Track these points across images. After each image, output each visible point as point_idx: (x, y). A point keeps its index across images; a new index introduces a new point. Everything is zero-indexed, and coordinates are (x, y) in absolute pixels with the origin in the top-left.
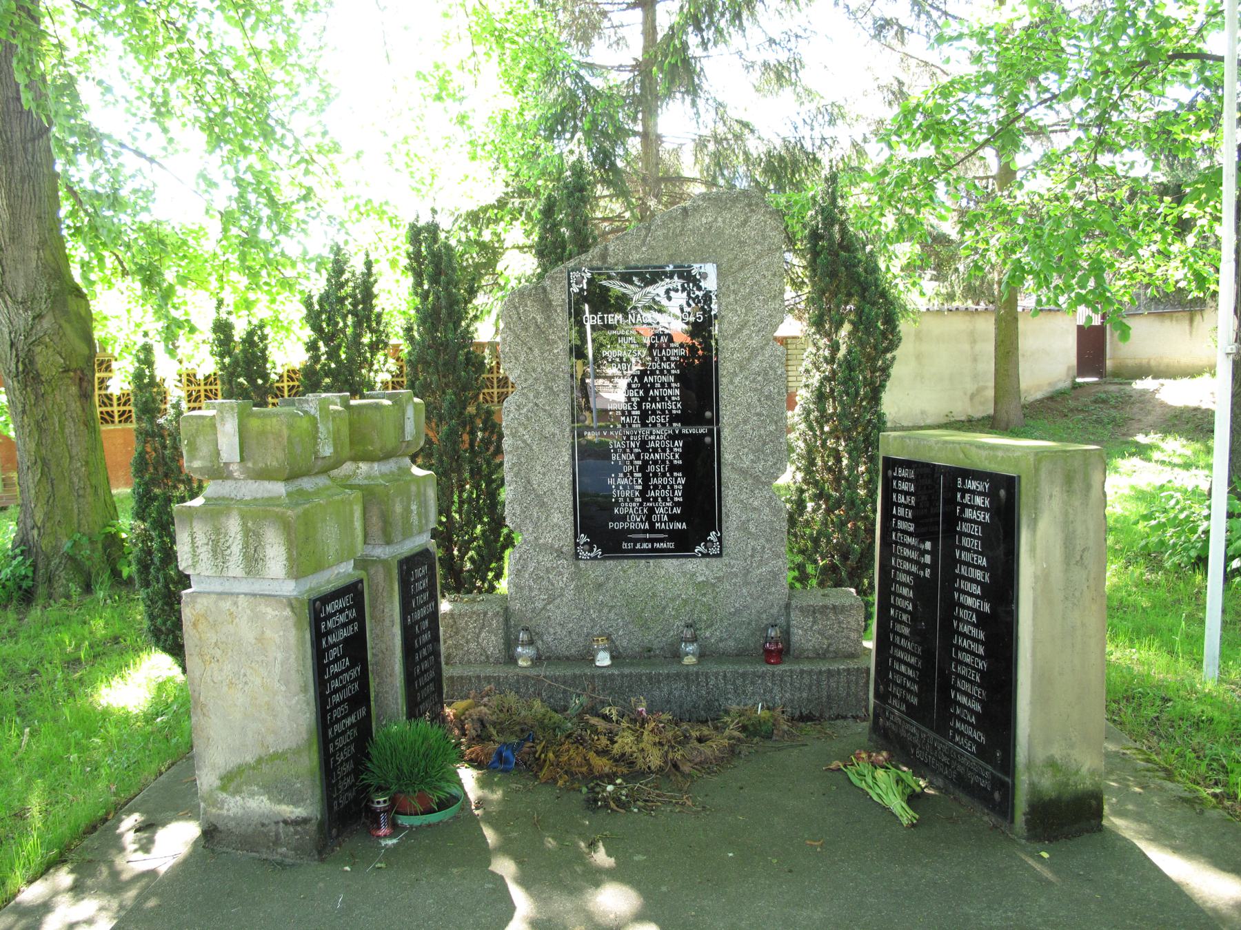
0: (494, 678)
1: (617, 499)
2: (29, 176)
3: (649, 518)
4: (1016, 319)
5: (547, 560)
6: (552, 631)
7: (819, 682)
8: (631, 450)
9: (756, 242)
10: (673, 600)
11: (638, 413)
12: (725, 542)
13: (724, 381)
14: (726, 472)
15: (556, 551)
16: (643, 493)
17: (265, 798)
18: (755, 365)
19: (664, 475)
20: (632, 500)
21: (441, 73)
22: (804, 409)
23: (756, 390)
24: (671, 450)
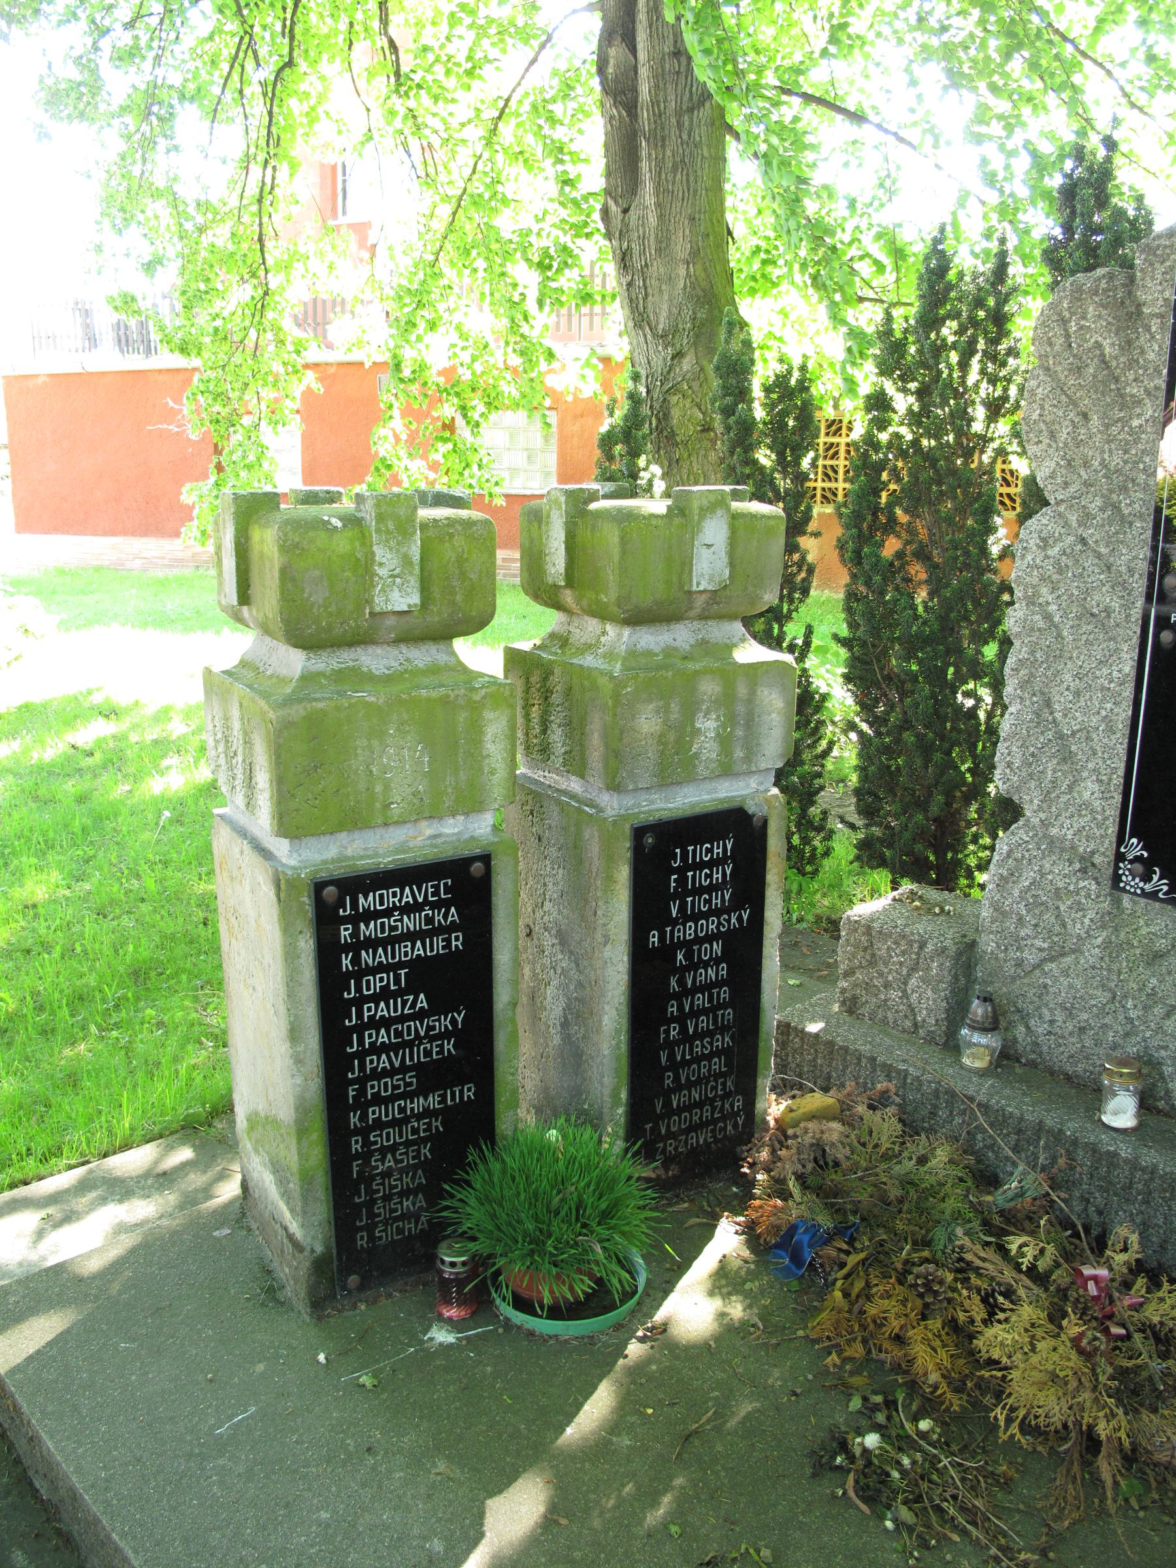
0: (898, 1072)
2: (683, 161)
5: (1059, 871)
6: (1047, 1015)
15: (1082, 859)
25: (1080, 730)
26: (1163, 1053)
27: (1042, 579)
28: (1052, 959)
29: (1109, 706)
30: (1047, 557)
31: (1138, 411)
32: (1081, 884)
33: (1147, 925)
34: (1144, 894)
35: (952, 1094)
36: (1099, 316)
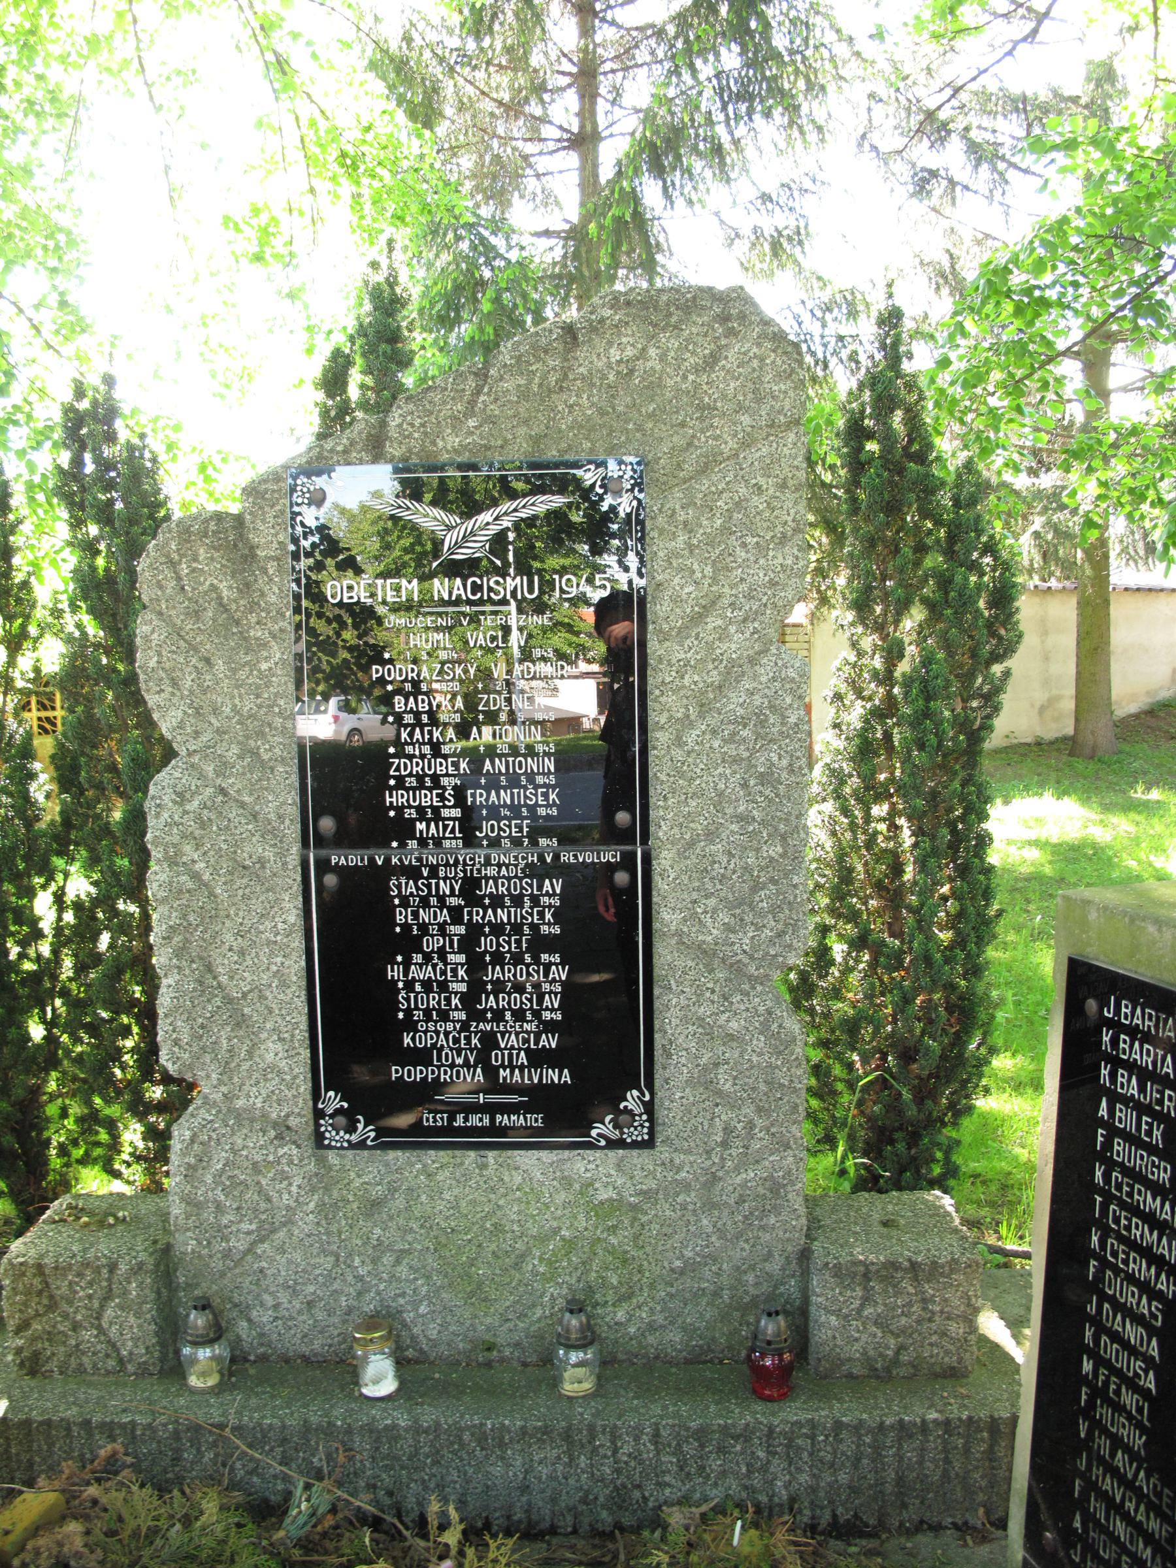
0: (123, 1426)
1: (408, 1012)
3: (483, 1058)
4: (1107, 603)
5: (254, 1144)
6: (268, 1300)
7: (877, 1448)
9: (740, 408)
10: (543, 1239)
11: (456, 813)
12: (660, 1114)
13: (660, 738)
14: (665, 954)
15: (275, 1125)
16: (469, 1001)
18: (735, 703)
19: (517, 959)
20: (444, 1016)
21: (263, 219)
22: (833, 772)
23: (736, 760)
24: (535, 900)
25: (251, 991)
26: (401, 1301)
27: (184, 836)
28: (262, 1240)
29: (279, 960)
30: (186, 812)
31: (265, 654)
32: (281, 1152)
33: (359, 1176)
34: (352, 1146)
35: (197, 1429)
36: (212, 559)
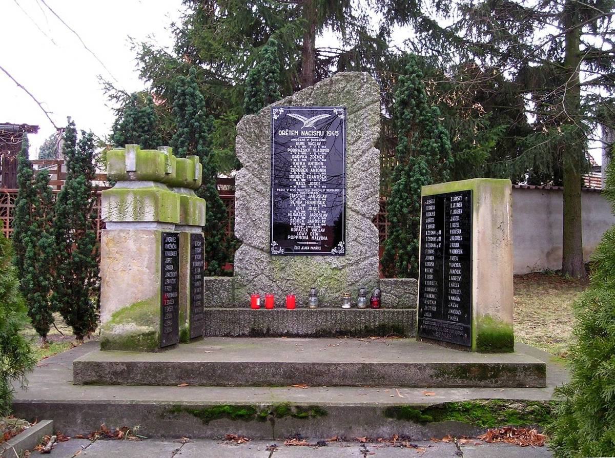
1: (292, 224)
3: (308, 234)
8: (301, 198)
16: (306, 221)
17: (134, 324)
18: (364, 158)
